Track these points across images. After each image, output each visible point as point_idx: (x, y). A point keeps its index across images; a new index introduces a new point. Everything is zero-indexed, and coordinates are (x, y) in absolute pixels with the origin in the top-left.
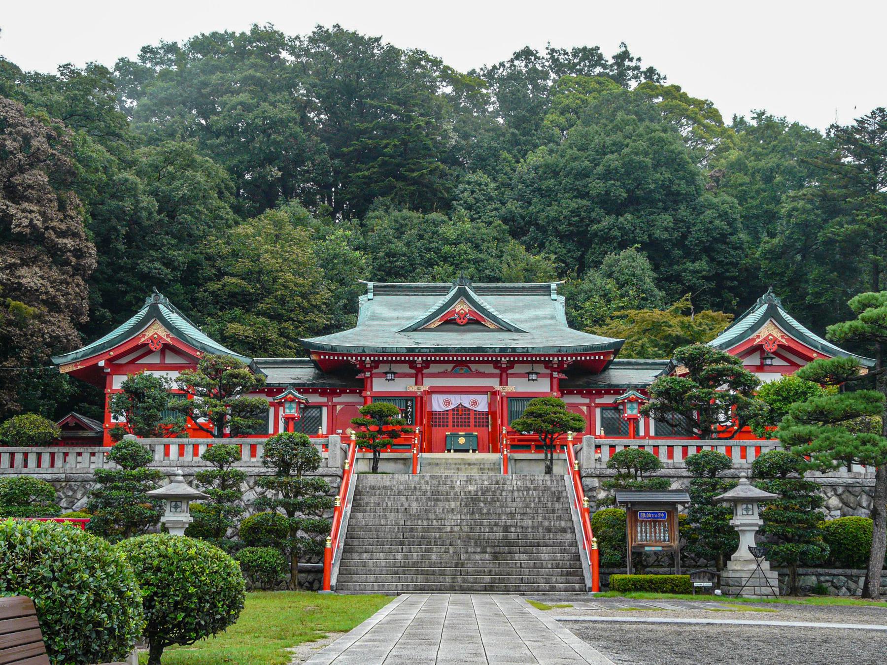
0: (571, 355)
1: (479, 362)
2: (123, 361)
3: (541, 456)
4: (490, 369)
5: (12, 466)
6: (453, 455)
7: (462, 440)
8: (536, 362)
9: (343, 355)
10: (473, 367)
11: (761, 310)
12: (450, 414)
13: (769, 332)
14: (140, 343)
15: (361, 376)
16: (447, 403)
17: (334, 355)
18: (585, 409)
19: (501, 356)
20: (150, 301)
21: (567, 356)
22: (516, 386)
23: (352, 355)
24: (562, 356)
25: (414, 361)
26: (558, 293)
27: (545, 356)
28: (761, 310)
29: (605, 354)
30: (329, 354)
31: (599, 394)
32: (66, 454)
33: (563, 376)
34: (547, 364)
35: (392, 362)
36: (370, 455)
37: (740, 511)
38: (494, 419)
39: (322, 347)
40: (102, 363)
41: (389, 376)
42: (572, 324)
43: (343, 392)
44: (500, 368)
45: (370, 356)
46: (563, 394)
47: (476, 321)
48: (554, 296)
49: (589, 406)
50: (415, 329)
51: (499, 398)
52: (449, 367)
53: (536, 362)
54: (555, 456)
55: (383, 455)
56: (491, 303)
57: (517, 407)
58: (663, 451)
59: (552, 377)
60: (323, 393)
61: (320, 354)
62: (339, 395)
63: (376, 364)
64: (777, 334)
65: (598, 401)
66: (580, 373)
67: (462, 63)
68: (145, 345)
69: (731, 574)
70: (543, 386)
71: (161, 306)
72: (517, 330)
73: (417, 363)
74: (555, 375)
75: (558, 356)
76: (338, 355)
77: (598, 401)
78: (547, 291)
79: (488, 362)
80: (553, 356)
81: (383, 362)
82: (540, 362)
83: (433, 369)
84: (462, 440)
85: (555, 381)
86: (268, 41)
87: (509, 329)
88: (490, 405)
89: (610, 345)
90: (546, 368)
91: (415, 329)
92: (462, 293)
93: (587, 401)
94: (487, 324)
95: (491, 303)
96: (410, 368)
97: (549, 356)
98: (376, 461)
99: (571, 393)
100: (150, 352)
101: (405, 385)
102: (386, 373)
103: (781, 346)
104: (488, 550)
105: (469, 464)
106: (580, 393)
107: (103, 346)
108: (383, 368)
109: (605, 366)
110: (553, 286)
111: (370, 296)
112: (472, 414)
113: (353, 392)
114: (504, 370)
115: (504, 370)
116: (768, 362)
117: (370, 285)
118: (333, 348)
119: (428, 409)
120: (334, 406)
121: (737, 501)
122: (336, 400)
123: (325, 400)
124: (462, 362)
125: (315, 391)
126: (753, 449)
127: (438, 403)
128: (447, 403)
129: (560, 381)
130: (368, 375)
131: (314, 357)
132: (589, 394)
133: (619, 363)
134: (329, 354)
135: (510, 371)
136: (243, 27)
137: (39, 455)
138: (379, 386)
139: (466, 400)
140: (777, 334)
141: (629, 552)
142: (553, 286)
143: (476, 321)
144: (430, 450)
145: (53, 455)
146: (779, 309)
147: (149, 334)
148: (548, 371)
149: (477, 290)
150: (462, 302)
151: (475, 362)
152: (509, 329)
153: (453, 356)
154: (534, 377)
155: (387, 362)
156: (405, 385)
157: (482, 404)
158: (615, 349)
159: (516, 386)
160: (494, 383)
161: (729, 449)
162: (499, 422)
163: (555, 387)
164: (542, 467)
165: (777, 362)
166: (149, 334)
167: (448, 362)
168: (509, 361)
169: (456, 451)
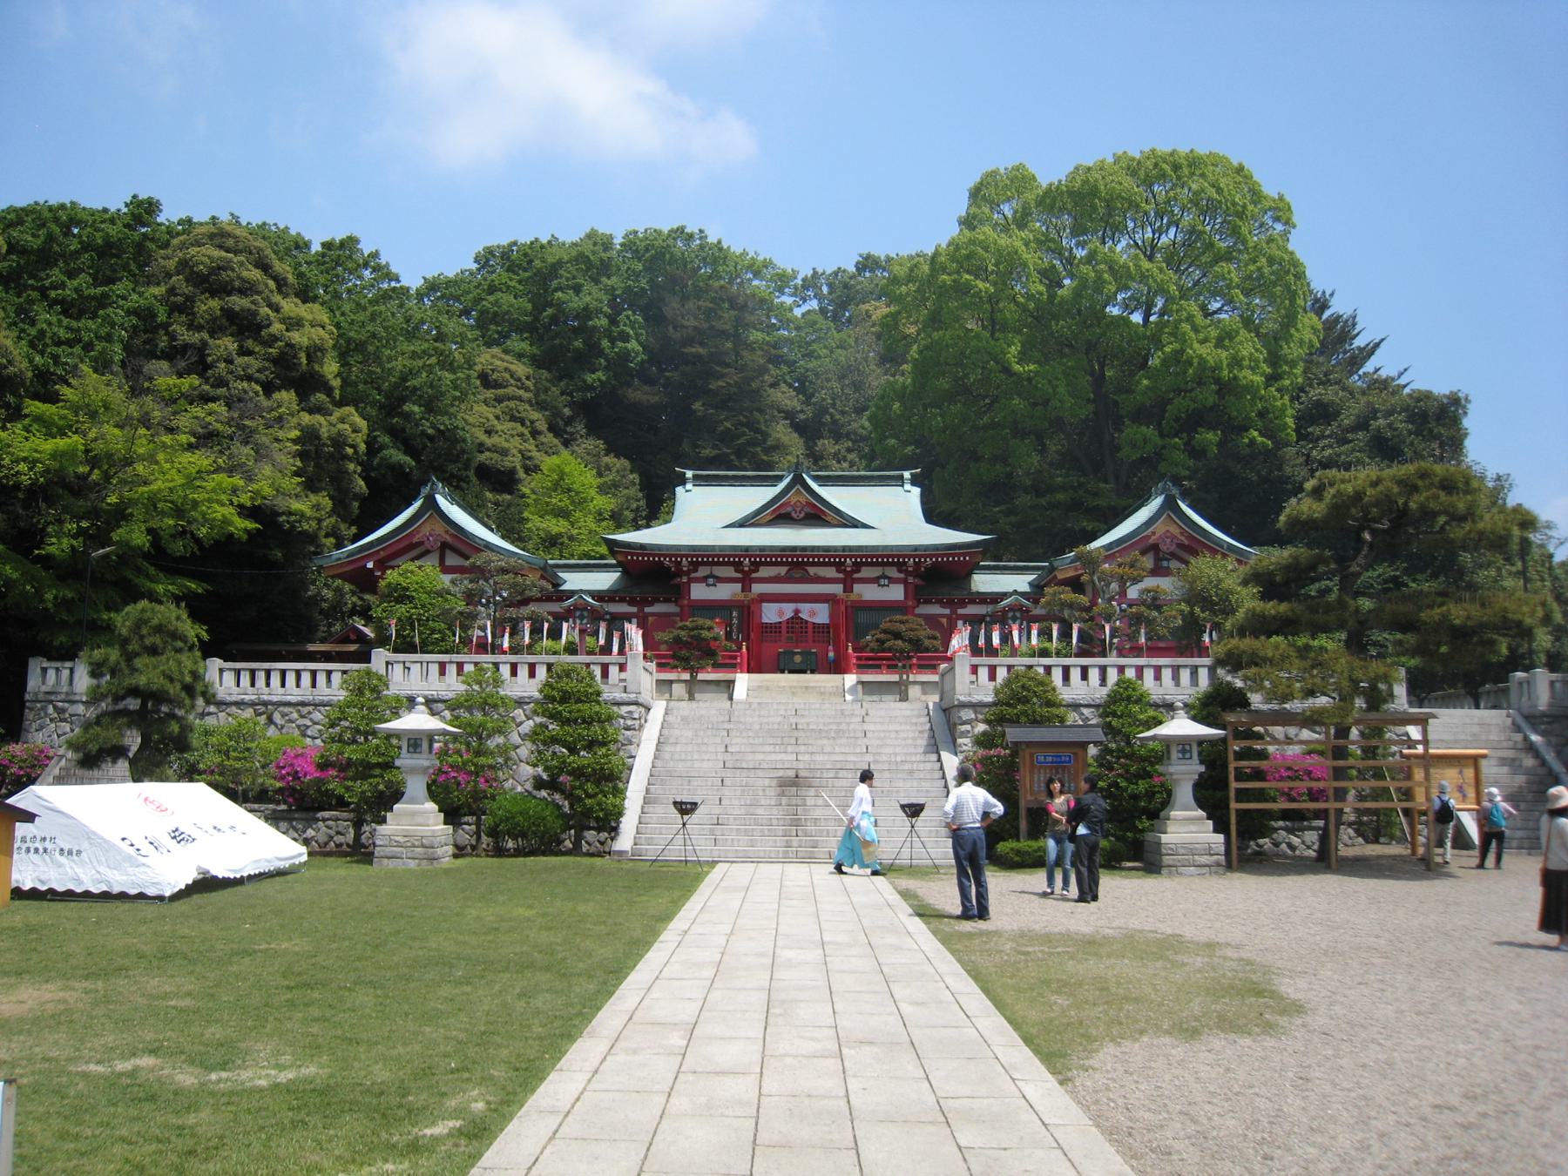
0: (931, 556)
7: (798, 659)
8: (888, 564)
9: (654, 555)
10: (812, 570)
11: (1156, 503)
16: (781, 613)
17: (643, 555)
18: (944, 621)
20: (425, 491)
21: (926, 556)
23: (665, 556)
24: (920, 556)
26: (913, 484)
27: (898, 556)
30: (638, 555)
31: (963, 604)
34: (901, 566)
40: (370, 565)
41: (711, 581)
43: (656, 601)
44: (844, 571)
45: (687, 556)
47: (819, 515)
48: (908, 487)
50: (742, 524)
52: (783, 570)
56: (834, 496)
58: (1057, 675)
60: (632, 602)
62: (651, 604)
63: (695, 566)
65: (961, 611)
66: (936, 577)
67: (799, 260)
68: (421, 543)
71: (439, 498)
72: (865, 526)
73: (744, 563)
74: (911, 580)
75: (914, 557)
76: (649, 555)
77: (961, 611)
78: (899, 481)
80: (909, 557)
81: (703, 564)
82: (892, 564)
83: (764, 572)
84: (798, 659)
85: (911, 588)
86: (599, 241)
87: (854, 524)
88: (832, 616)
90: (900, 571)
91: (742, 524)
93: (947, 611)
95: (834, 496)
97: (904, 556)
99: (927, 602)
101: (725, 592)
106: (940, 602)
108: (703, 571)
111: (689, 486)
113: (667, 600)
116: (1165, 564)
117: (689, 474)
122: (647, 610)
124: (797, 563)
125: (622, 600)
126: (1188, 671)
128: (781, 613)
133: (985, 568)
136: (571, 233)
138: (699, 592)
139: (806, 610)
140: (1174, 530)
141: (1023, 813)
142: (907, 475)
143: (819, 515)
149: (815, 478)
152: (854, 524)
155: (708, 564)
160: (837, 589)
161: (1140, 670)
166: (426, 530)
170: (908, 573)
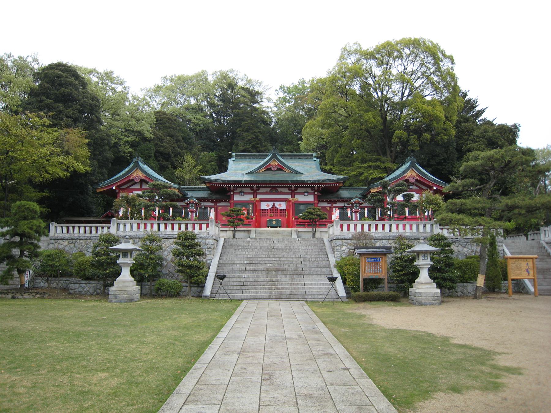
1: (282, 187)
2: (124, 187)
3: (311, 229)
4: (286, 190)
5: (68, 232)
6: (270, 229)
10: (279, 190)
11: (408, 164)
12: (269, 211)
13: (411, 175)
14: (131, 178)
15: (229, 194)
17: (216, 184)
18: (328, 208)
19: (292, 184)
20: (135, 160)
22: (300, 198)
25: (314, 187)
28: (408, 164)
29: (339, 183)
30: (214, 184)
31: (335, 202)
32: (103, 228)
33: (319, 194)
34: (312, 188)
35: (243, 187)
36: (232, 229)
37: (421, 257)
38: (289, 213)
39: (210, 180)
40: (114, 188)
41: (306, 194)
42: (323, 170)
43: (221, 201)
44: (291, 190)
46: (319, 202)
49: (330, 207)
51: (291, 204)
52: (268, 190)
53: (308, 187)
54: (317, 229)
55: (238, 229)
57: (299, 207)
59: (314, 194)
60: (212, 202)
61: (210, 183)
62: (220, 202)
64: (415, 175)
65: (334, 205)
68: (133, 180)
69: (417, 291)
70: (311, 198)
73: (253, 187)
74: (316, 193)
75: (317, 184)
76: (218, 184)
77: (334, 205)
79: (286, 187)
83: (261, 190)
84: (274, 222)
85: (316, 196)
87: (296, 172)
89: (341, 179)
90: (289, 190)
92: (274, 157)
93: (330, 205)
94: (285, 170)
96: (251, 190)
98: (235, 231)
99: (323, 201)
100: (136, 183)
101: (248, 198)
102: (305, 192)
103: (417, 180)
104: (288, 276)
105: (278, 233)
106: (327, 201)
107: (116, 179)
109: (338, 189)
110: (314, 154)
112: (279, 210)
113: (225, 201)
114: (293, 191)
115: (293, 191)
118: (303, 181)
119: (258, 209)
120: (218, 207)
121: (419, 253)
122: (218, 205)
123: (213, 204)
125: (209, 201)
127: (264, 206)
129: (318, 196)
130: (232, 193)
131: (208, 185)
132: (331, 202)
134: (214, 184)
135: (258, 191)
137: (85, 228)
139: (277, 204)
140: (415, 175)
144: (260, 227)
145: (97, 228)
146: (417, 165)
147: (135, 174)
148: (313, 192)
149: (283, 157)
150: (274, 161)
151: (280, 187)
153: (268, 184)
154: (242, 194)
156: (248, 198)
157: (282, 206)
158: (343, 181)
159: (300, 198)
160: (289, 197)
162: (291, 214)
163: (316, 198)
164: (311, 235)
165: (414, 187)
167: (268, 187)
168: (295, 187)
169: (271, 227)
170: (315, 191)
